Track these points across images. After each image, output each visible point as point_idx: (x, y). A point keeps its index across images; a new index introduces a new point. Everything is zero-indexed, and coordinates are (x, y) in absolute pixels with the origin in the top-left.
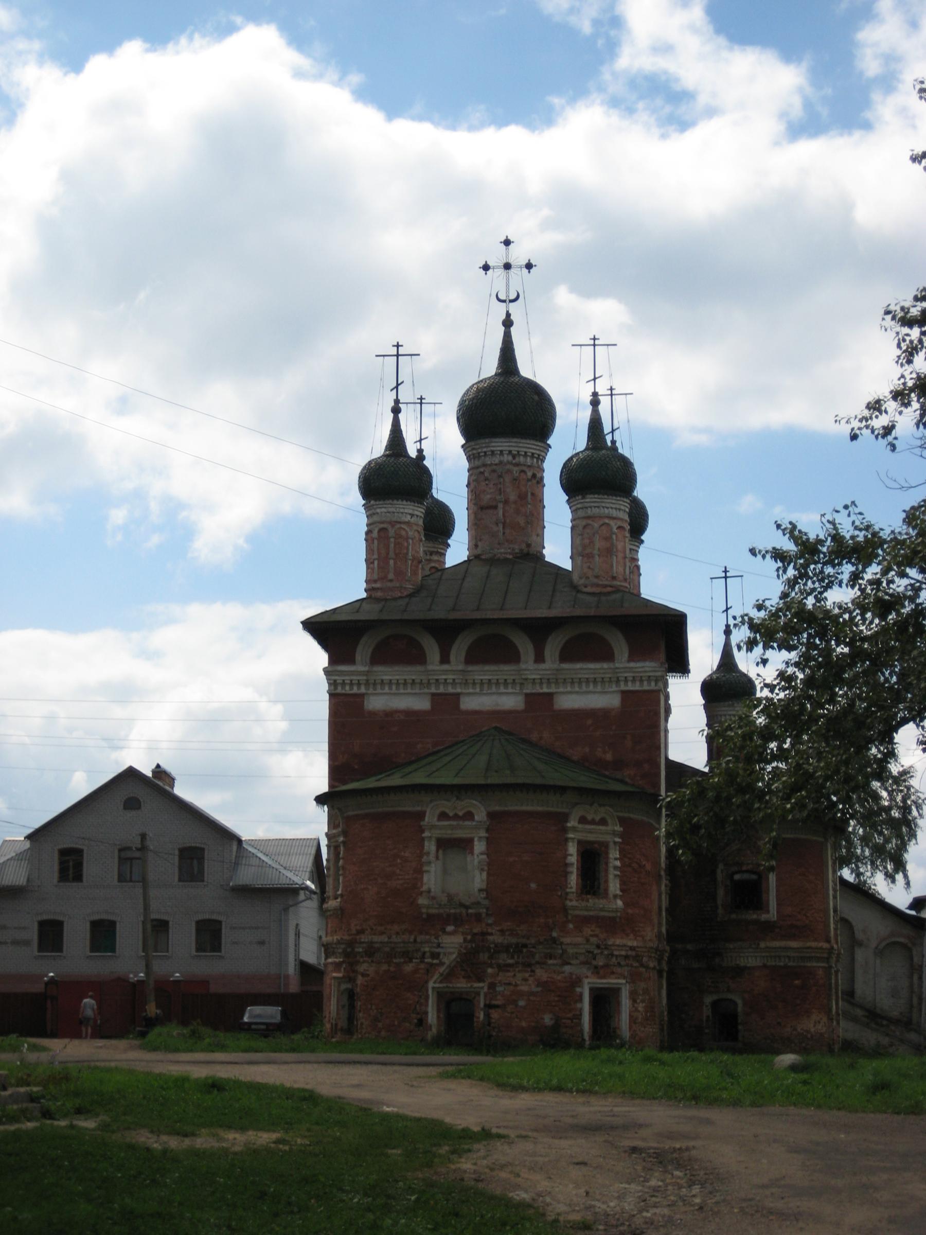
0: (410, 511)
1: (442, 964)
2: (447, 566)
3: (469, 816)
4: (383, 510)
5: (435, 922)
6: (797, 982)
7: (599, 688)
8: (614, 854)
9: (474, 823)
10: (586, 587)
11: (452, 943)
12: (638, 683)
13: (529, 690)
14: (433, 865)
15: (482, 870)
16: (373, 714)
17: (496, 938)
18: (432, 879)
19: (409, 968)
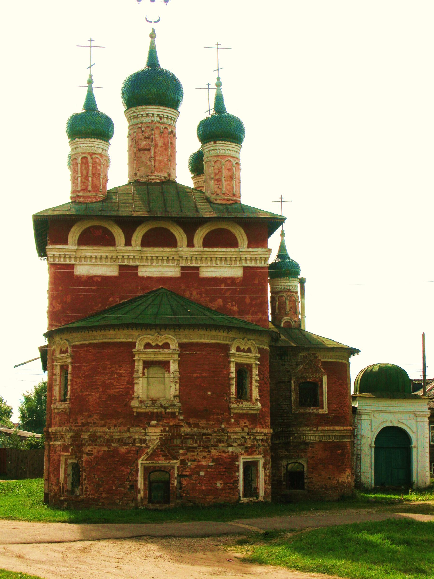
0: (102, 147)
1: (148, 447)
2: (110, 186)
3: (166, 346)
4: (85, 145)
5: (143, 419)
6: (339, 452)
7: (228, 264)
8: (255, 371)
9: (170, 351)
10: (216, 200)
11: (154, 434)
12: (253, 262)
13: (184, 263)
14: (141, 379)
15: (176, 382)
16: (79, 277)
17: (185, 430)
18: (141, 388)
19: (123, 450)
